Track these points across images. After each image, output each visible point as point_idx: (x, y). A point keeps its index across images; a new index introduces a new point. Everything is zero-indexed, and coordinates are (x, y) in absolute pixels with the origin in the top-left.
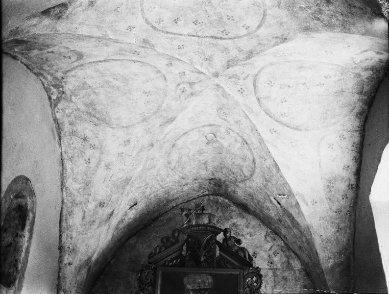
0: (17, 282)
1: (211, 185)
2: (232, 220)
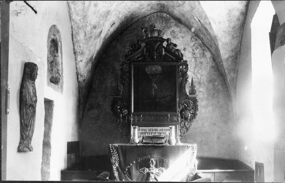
0: (61, 81)
1: (158, 7)
2: (171, 28)
